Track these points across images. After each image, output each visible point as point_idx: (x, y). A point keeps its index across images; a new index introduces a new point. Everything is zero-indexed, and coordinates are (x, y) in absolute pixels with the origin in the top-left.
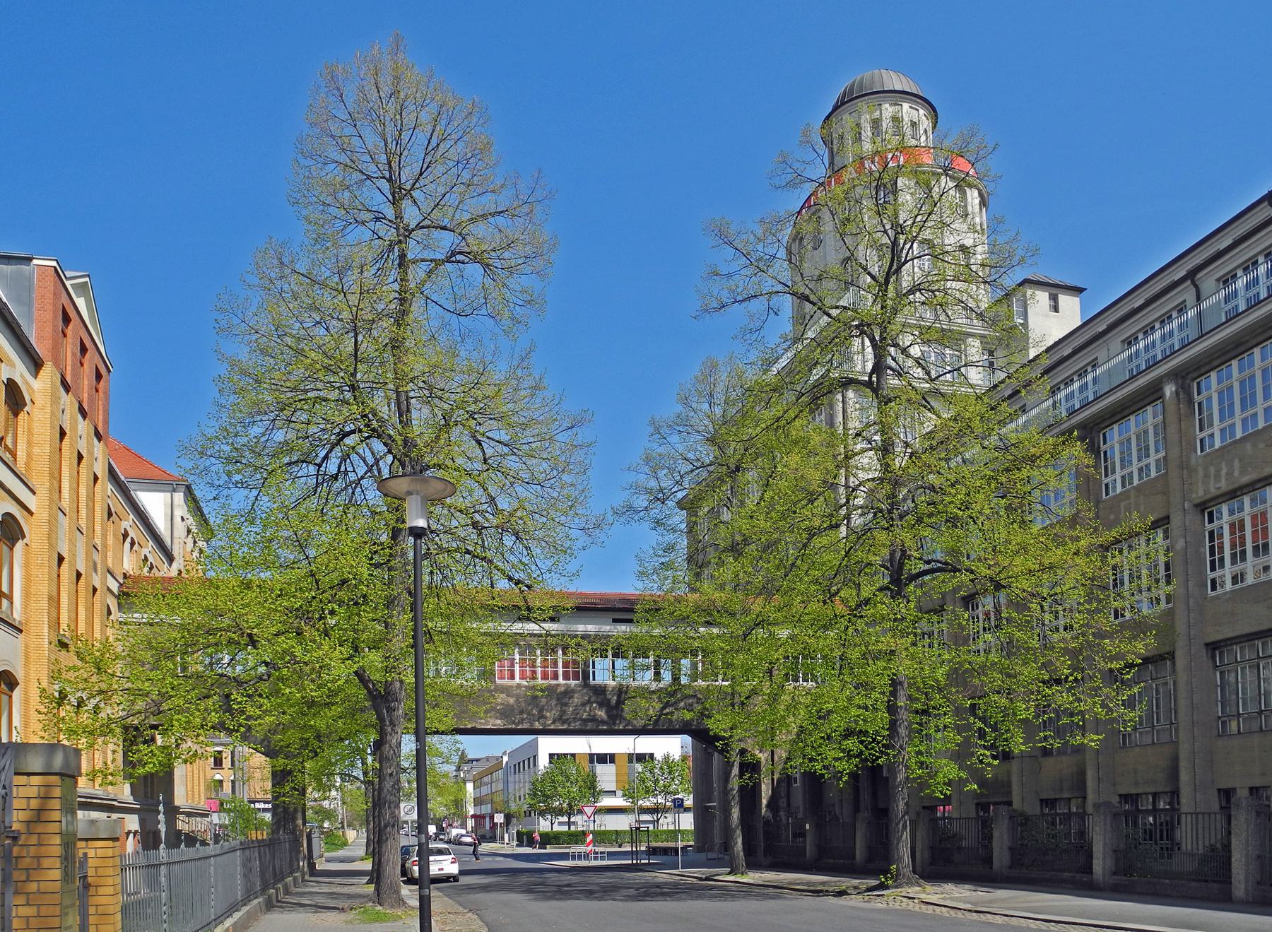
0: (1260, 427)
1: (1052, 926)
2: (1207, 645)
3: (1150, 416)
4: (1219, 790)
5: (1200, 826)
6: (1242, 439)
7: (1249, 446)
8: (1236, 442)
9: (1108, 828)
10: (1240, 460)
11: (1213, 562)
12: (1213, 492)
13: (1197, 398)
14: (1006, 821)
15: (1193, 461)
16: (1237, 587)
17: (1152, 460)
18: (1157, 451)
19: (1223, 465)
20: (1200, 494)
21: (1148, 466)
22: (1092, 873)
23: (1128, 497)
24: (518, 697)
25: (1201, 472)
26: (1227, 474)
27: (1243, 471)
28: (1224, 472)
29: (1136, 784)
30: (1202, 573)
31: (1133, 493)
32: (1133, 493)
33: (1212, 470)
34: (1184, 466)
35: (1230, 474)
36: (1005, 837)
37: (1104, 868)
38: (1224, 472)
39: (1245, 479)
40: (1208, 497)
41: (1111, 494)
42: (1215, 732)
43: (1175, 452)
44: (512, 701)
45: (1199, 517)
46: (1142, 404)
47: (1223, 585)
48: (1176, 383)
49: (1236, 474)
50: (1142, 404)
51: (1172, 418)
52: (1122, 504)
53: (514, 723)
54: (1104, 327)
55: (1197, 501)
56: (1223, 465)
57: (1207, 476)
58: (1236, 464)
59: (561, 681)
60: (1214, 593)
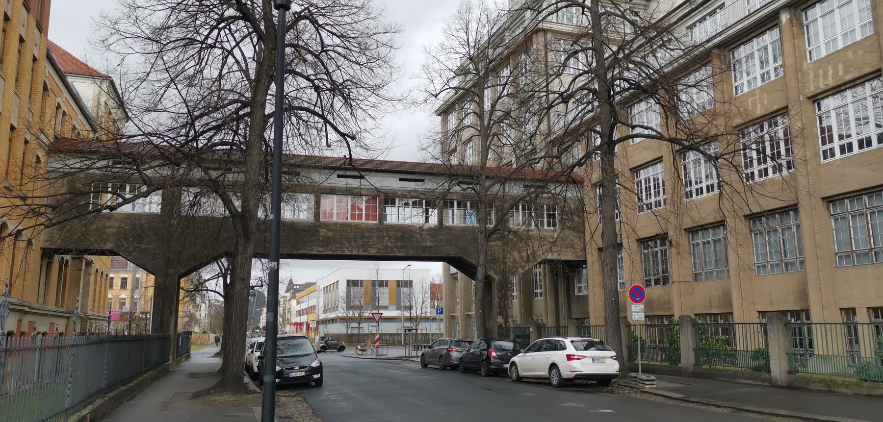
0: (840, 48)
1: (765, 417)
2: (823, 199)
3: (770, 38)
4: (841, 309)
5: (829, 337)
6: (843, 49)
7: (850, 54)
8: (839, 51)
9: (781, 334)
10: (843, 64)
11: (823, 139)
12: (823, 87)
13: (805, 22)
14: (690, 327)
15: (805, 67)
16: (862, 151)
17: (771, 66)
18: (775, 60)
19: (830, 68)
20: (812, 89)
21: (768, 73)
22: (769, 372)
23: (754, 95)
24: (334, 231)
25: (812, 76)
26: (833, 74)
27: (846, 72)
28: (831, 72)
29: (772, 303)
30: (816, 146)
31: (758, 92)
32: (758, 92)
33: (821, 72)
34: (798, 70)
35: (835, 74)
36: (690, 339)
37: (780, 367)
38: (831, 72)
39: (848, 77)
40: (818, 91)
41: (740, 94)
42: (834, 265)
43: (790, 61)
44: (330, 234)
45: (812, 106)
46: (763, 30)
47: (833, 155)
48: (790, 13)
49: (841, 74)
50: (763, 30)
51: (787, 36)
52: (750, 100)
53: (331, 250)
54: (676, 19)
55: (810, 95)
56: (830, 68)
57: (817, 76)
58: (840, 66)
59: (364, 220)
60: (826, 161)
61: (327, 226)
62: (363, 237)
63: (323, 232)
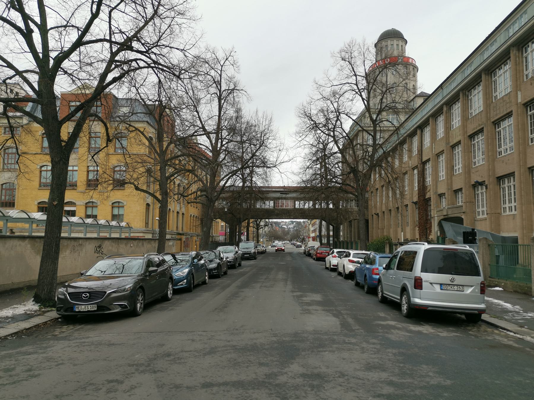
61: (277, 210)
62: (289, 213)
63: (276, 211)
